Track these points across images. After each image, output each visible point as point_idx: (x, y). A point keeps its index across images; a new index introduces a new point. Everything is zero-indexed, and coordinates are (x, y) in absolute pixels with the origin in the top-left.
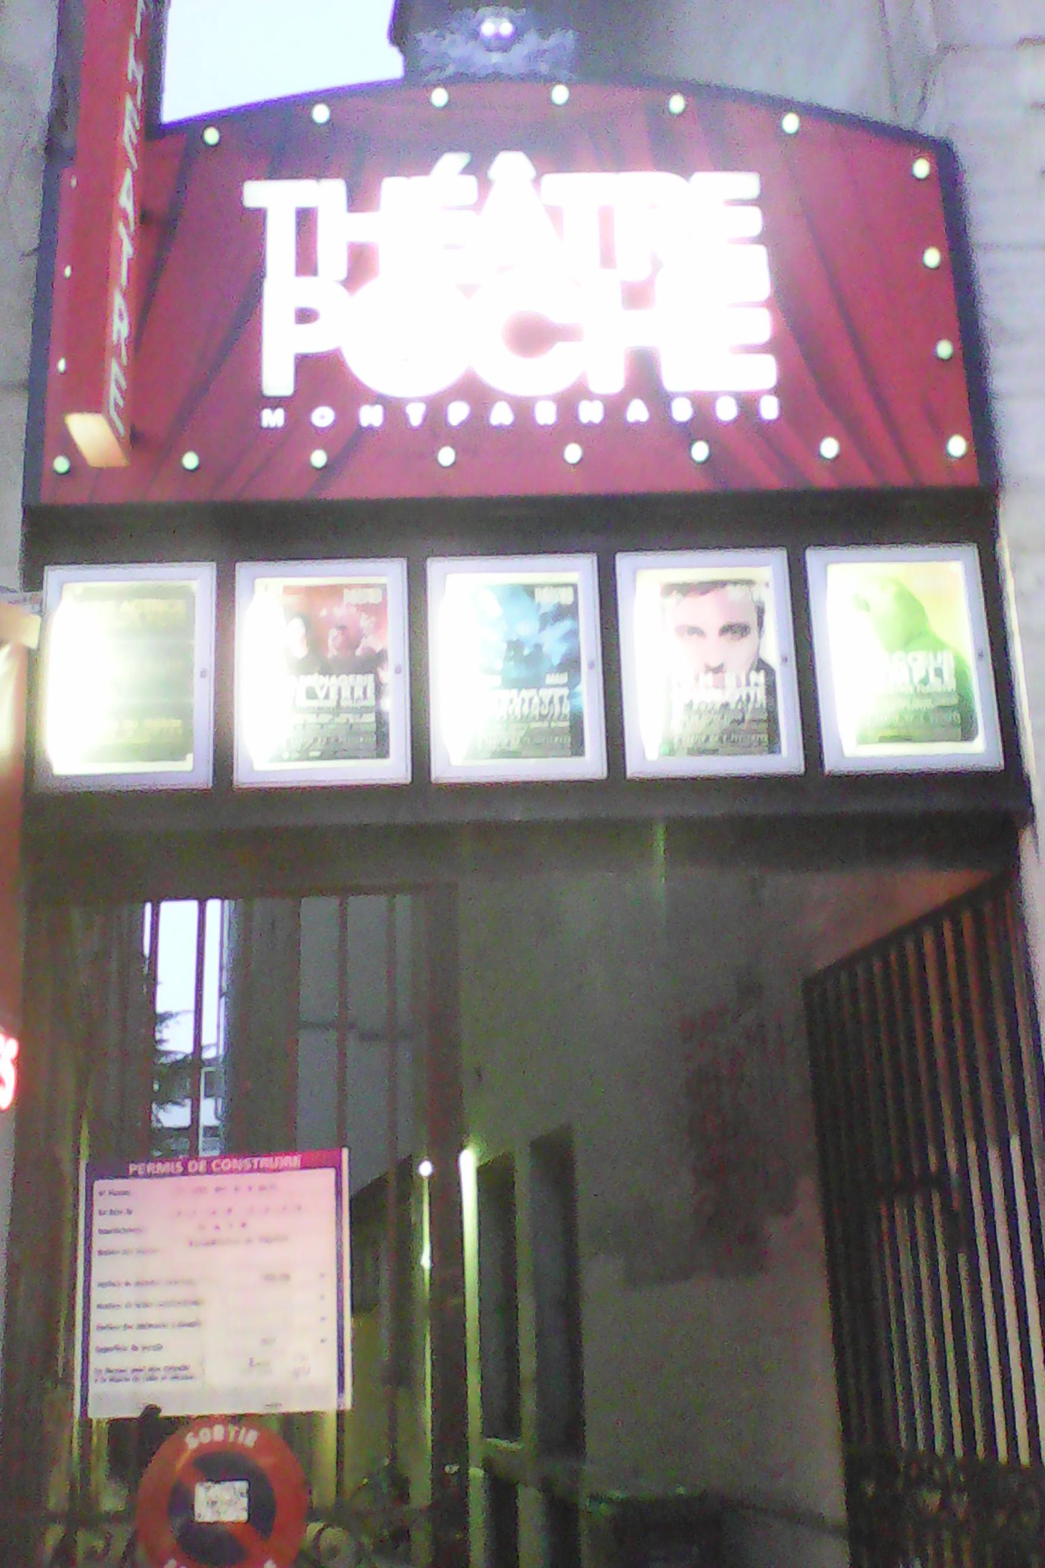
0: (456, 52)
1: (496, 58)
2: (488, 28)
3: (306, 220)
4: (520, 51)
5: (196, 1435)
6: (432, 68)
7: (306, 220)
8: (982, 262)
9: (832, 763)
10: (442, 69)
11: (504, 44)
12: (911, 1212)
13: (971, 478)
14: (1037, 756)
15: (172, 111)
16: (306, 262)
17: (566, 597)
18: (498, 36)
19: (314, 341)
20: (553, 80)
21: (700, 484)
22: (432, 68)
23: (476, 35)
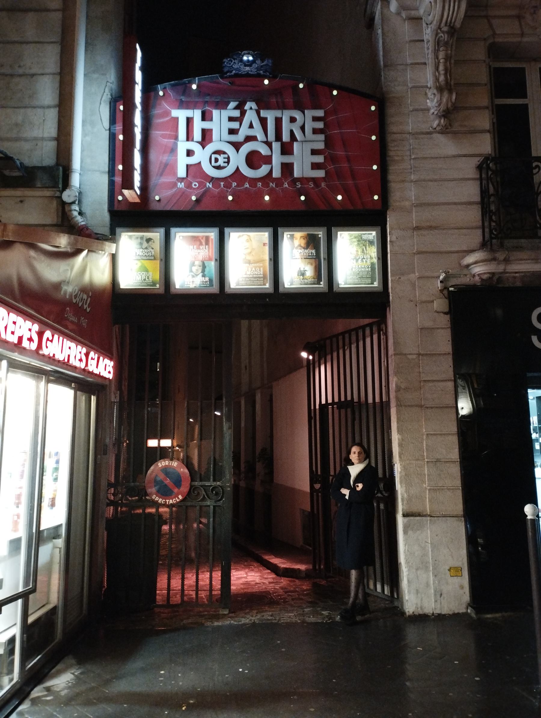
0: (235, 66)
1: (248, 68)
2: (245, 58)
3: (189, 121)
4: (255, 66)
5: (76, 217)
6: (228, 72)
7: (189, 121)
8: (389, 138)
9: (227, 290)
10: (231, 72)
11: (249, 64)
12: (346, 412)
13: (379, 207)
14: (392, 288)
15: (41, 529)
16: (189, 137)
17: (289, 236)
18: (248, 61)
19: (192, 160)
20: (265, 77)
21: (303, 208)
22: (228, 72)
23: (241, 61)
